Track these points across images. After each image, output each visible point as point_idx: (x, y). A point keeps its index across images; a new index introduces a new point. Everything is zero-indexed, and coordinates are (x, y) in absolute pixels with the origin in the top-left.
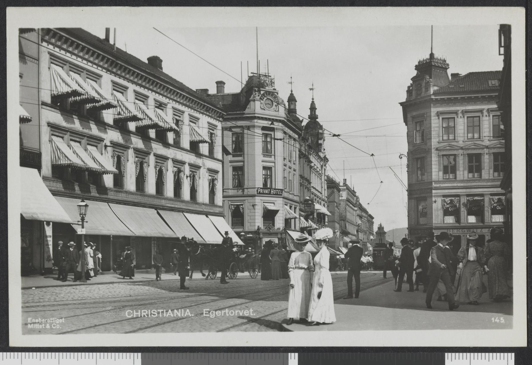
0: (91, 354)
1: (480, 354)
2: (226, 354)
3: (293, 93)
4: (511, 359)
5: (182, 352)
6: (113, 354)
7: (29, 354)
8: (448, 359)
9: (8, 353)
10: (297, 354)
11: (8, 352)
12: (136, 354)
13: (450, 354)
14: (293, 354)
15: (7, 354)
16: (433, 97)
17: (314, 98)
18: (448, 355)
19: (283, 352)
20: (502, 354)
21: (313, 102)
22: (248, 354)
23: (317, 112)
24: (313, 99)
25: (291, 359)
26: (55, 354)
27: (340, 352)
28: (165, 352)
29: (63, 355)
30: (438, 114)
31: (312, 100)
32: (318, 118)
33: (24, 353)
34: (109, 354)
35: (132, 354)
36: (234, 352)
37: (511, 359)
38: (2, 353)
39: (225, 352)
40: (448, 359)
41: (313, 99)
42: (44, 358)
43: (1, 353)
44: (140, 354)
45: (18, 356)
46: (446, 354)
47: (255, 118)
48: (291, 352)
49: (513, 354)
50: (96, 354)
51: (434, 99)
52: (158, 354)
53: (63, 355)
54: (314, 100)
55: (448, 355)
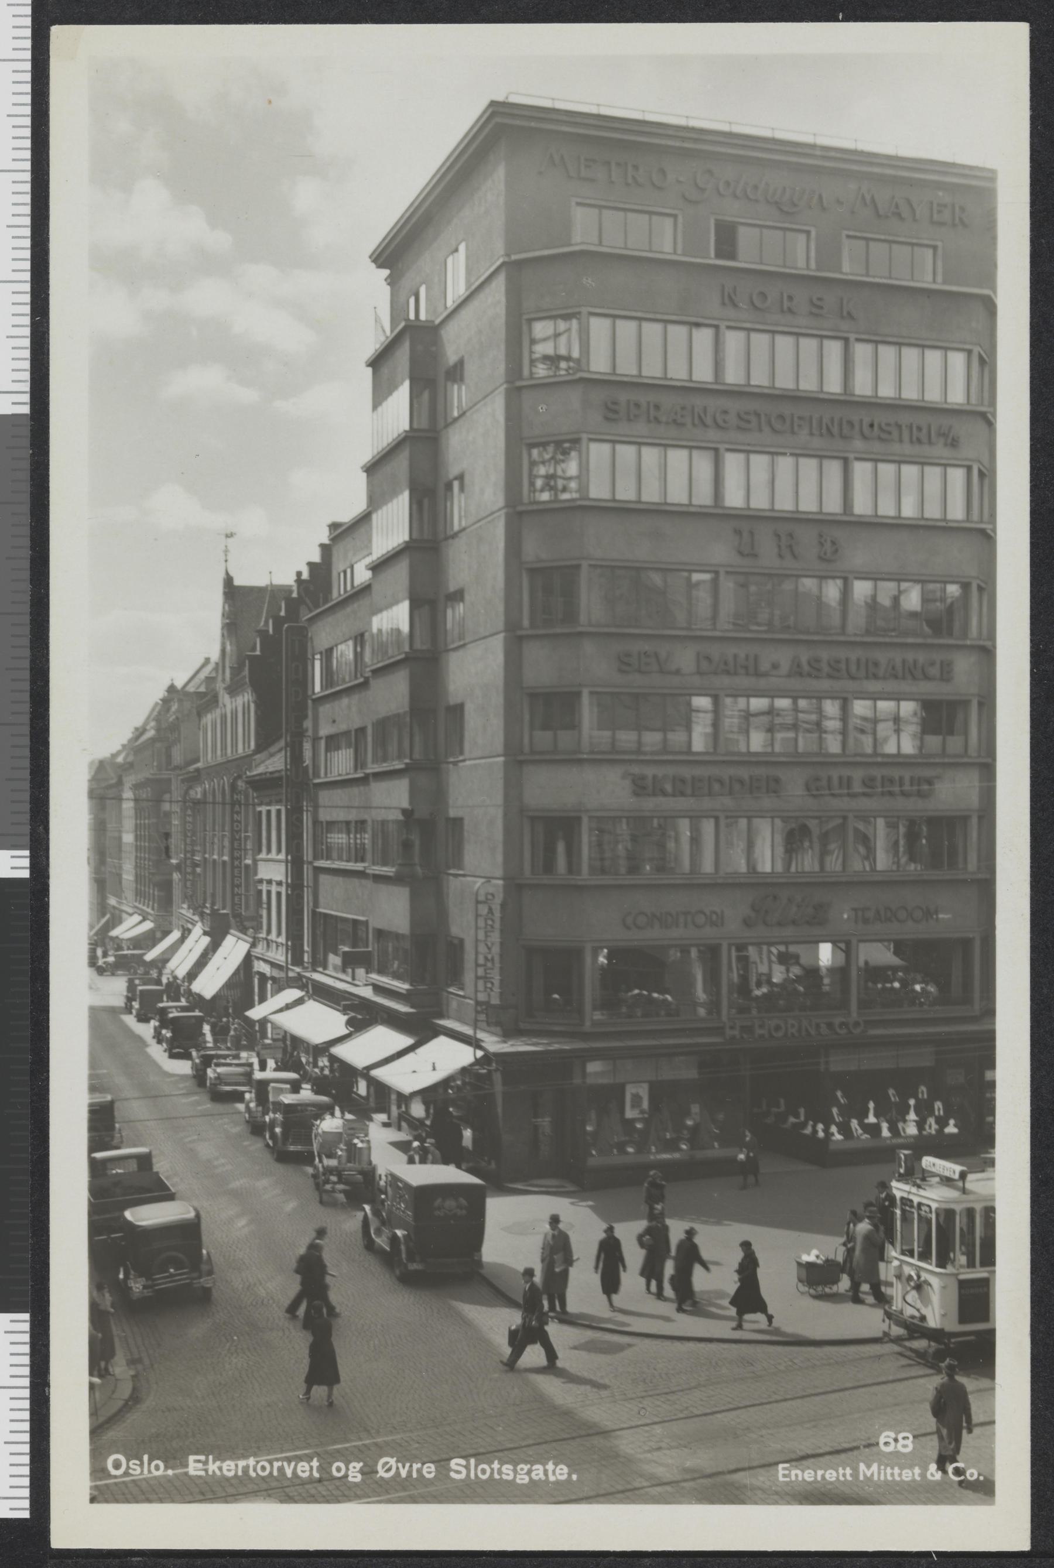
0: (27, 265)
2: (27, 664)
4: (11, 1509)
7: (27, 94)
8: (12, 1321)
9: (28, 21)
10: (26, 874)
11: (33, 21)
13: (27, 1327)
14: (26, 863)
15: (26, 16)
19: (31, 834)
20: (26, 1482)
22: (26, 730)
25: (13, 857)
26: (27, 127)
27: (32, 1002)
29: (22, 182)
36: (32, 689)
37: (11, 1509)
40: (12, 1321)
42: (14, 182)
44: (26, 410)
45: (20, 49)
46: (26, 1316)
48: (33, 858)
49: (26, 1515)
53: (22, 182)
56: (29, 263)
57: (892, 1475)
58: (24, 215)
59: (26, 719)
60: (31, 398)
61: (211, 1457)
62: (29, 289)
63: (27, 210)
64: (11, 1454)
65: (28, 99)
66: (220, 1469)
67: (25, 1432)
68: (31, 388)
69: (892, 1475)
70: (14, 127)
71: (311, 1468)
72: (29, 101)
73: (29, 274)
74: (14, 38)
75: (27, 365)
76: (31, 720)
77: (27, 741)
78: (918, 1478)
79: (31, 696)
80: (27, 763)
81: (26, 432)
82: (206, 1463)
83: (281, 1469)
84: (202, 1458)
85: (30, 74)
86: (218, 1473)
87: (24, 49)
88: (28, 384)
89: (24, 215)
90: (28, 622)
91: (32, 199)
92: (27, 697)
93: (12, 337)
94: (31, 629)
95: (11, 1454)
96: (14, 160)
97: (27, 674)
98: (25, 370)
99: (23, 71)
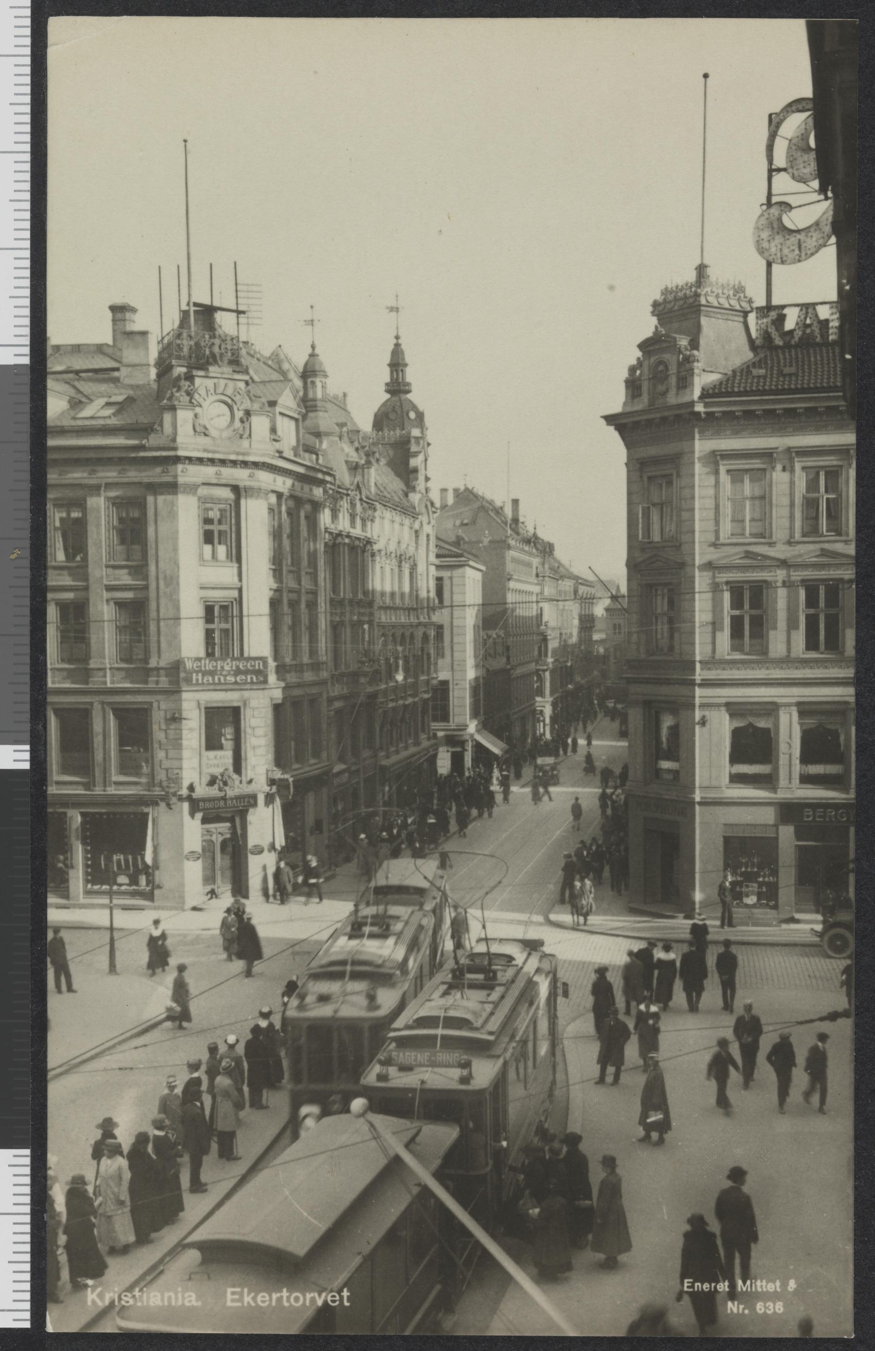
0: (27, 234)
1: (28, 1238)
2: (27, 582)
3: (317, 351)
4: (14, 1320)
5: (31, 471)
6: (27, 292)
7: (27, 85)
8: (15, 1156)
9: (28, 22)
10: (26, 766)
11: (32, 22)
12: (27, 350)
13: (27, 1161)
14: (27, 756)
15: (26, 17)
16: (699, 408)
17: (400, 334)
18: (26, 751)
19: (31, 731)
20: (28, 1296)
21: (397, 345)
22: (27, 640)
23: (411, 375)
24: (397, 338)
25: (15, 751)
26: (27, 143)
27: (32, 877)
28: (31, 426)
29: (22, 162)
30: (715, 458)
31: (395, 341)
32: (409, 392)
33: (29, 63)
34: (28, 138)
35: (27, 341)
36: (32, 604)
37: (14, 1320)
38: (29, 5)
39: (33, 580)
40: (15, 1156)
41: (397, 338)
42: (15, 259)
43: (28, 3)
44: (26, 361)
45: (21, 46)
46: (27, 1152)
47: (177, 460)
48: (32, 752)
49: (27, 1325)
50: (26, 249)
51: (703, 416)
52: (27, 408)
53: (22, 162)
54: (400, 341)
55: (26, 751)
56: (29, 232)
57: (761, 1286)
58: (25, 191)
59: (27, 630)
60: (31, 351)
61: (246, 1290)
62: (29, 236)
63: (27, 186)
64: (14, 1272)
65: (28, 89)
66: (254, 1299)
67: (26, 1253)
68: (31, 342)
69: (761, 1286)
70: (14, 1195)
71: (341, 1298)
72: (29, 92)
73: (29, 242)
74: (14, 1291)
75: (27, 321)
76: (31, 631)
77: (27, 650)
78: (778, 1290)
79: (31, 610)
80: (27, 669)
81: (27, 379)
82: (241, 1294)
83: (313, 1300)
84: (238, 1290)
85: (29, 68)
86: (253, 1304)
87: (25, 46)
88: (28, 338)
89: (25, 191)
90: (28, 546)
91: (31, 177)
92: (27, 611)
93: (14, 297)
94: (31, 553)
95: (14, 1272)
96: (16, 143)
97: (27, 592)
98: (25, 326)
99: (23, 65)
